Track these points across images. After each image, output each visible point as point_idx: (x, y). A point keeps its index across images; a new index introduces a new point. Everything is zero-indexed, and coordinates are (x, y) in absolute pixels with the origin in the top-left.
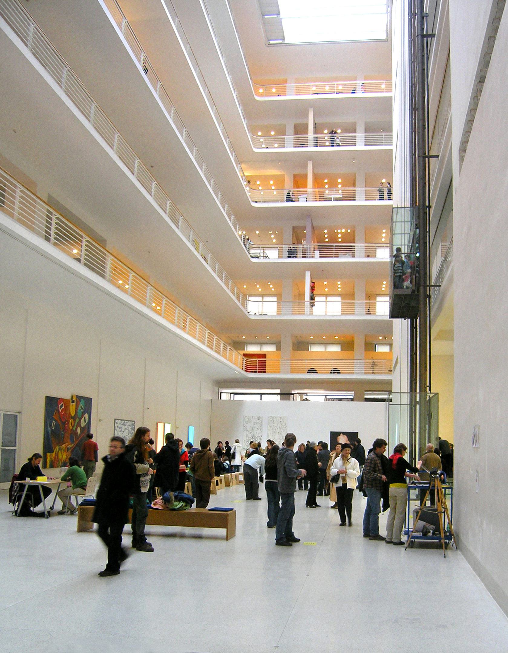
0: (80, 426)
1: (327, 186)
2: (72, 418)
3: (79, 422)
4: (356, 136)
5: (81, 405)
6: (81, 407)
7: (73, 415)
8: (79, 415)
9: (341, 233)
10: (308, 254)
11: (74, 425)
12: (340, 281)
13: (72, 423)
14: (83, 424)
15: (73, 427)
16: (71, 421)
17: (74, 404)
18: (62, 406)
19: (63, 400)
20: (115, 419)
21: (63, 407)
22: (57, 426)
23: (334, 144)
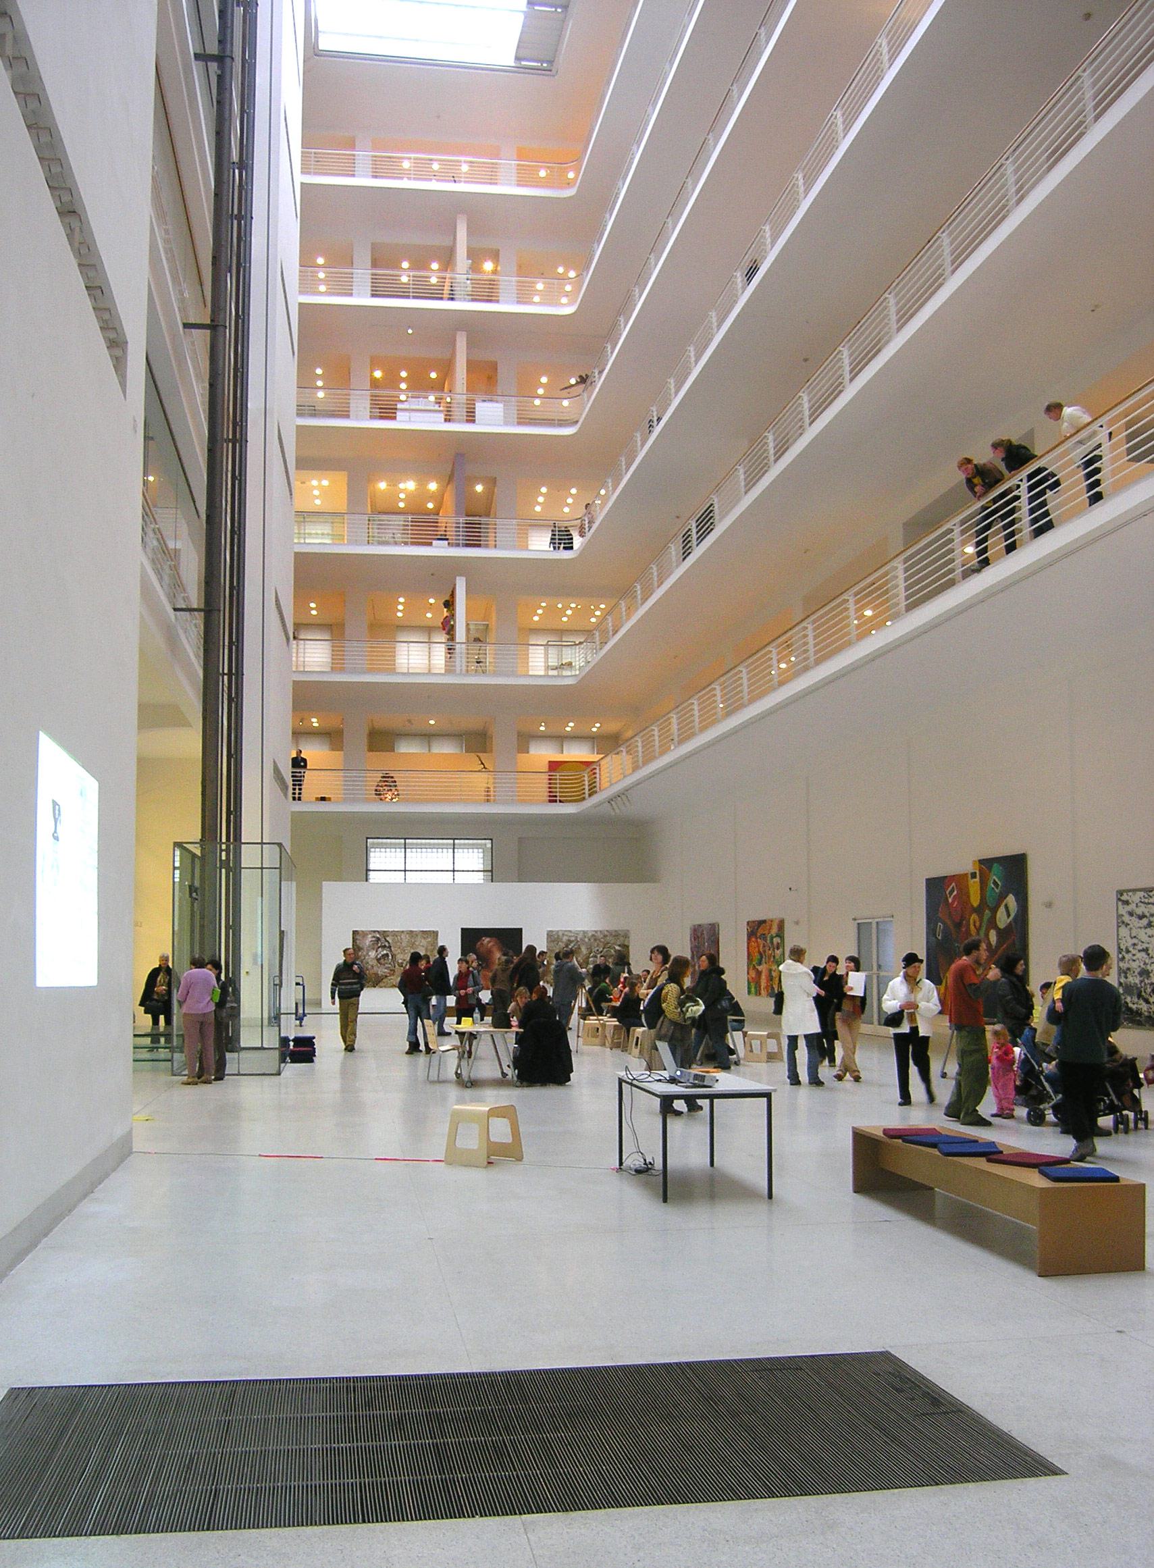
0: (996, 927)
1: (403, 386)
2: (975, 910)
3: (993, 917)
4: (352, 274)
5: (994, 877)
6: (995, 883)
7: (975, 903)
8: (990, 901)
9: (320, 488)
10: (461, 538)
11: (980, 926)
12: (404, 597)
13: (975, 922)
14: (1002, 920)
15: (978, 930)
16: (974, 917)
17: (977, 879)
18: (952, 891)
19: (952, 878)
20: (1121, 893)
21: (955, 893)
22: (946, 933)
23: (442, 294)
